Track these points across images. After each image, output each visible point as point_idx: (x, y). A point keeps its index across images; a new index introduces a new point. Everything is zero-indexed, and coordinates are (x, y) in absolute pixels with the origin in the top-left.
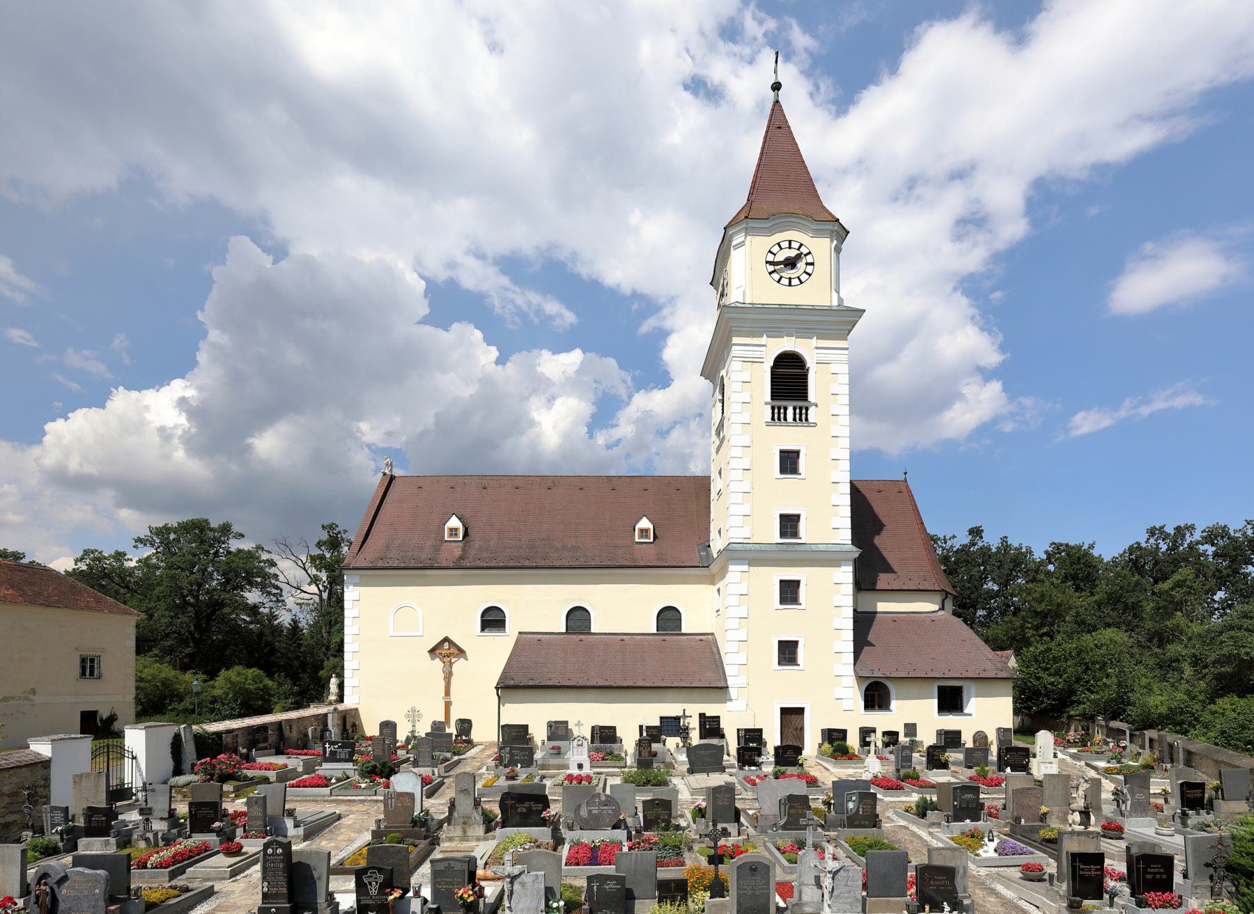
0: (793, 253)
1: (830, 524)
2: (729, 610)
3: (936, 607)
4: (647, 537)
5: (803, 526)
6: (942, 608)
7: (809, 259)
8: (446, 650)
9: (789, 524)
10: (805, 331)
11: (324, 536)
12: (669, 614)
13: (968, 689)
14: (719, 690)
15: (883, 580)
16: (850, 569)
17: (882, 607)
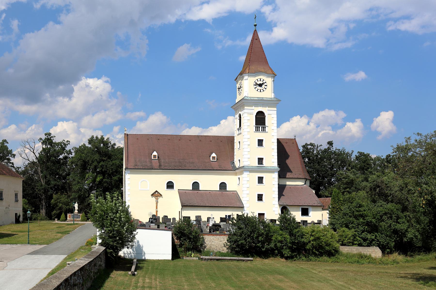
0: (261, 82)
1: (272, 160)
2: (243, 186)
3: (303, 184)
4: (215, 159)
5: (264, 161)
6: (305, 184)
7: (266, 84)
8: (156, 195)
9: (260, 161)
10: (264, 105)
11: (44, 137)
12: (224, 184)
13: (310, 209)
14: (242, 207)
15: (289, 175)
16: (277, 174)
17: (288, 183)
